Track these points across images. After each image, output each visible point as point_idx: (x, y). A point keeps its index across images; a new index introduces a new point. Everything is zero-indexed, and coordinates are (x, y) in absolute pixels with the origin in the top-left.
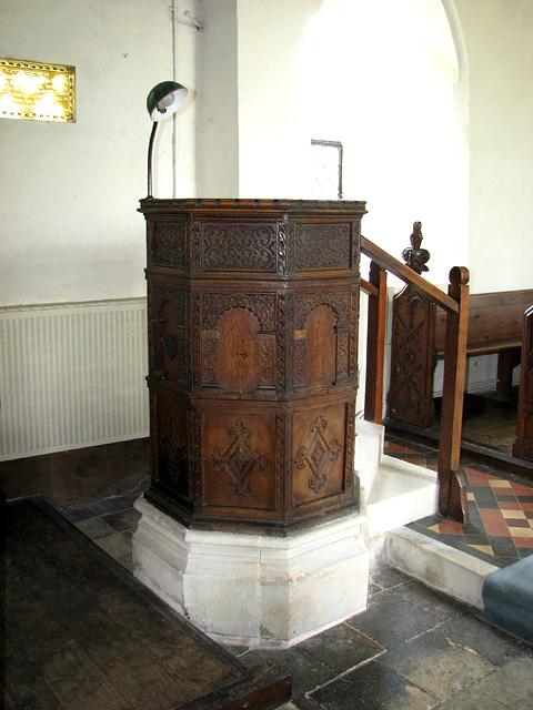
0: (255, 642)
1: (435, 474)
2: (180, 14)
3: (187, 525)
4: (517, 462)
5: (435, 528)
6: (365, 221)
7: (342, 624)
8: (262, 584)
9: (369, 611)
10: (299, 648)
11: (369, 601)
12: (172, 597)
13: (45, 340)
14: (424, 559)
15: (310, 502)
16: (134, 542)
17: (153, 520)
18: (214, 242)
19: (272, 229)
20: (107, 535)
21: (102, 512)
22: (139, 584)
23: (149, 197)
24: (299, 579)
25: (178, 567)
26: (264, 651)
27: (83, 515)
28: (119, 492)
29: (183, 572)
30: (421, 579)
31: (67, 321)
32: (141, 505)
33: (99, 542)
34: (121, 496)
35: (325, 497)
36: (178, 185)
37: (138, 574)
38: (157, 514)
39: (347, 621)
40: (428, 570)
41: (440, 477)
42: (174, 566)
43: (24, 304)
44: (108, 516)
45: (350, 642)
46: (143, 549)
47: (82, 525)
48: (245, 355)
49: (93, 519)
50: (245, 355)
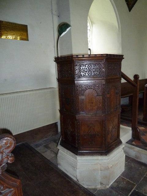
0: (99, 187)
1: (131, 128)
2: (54, 12)
3: (77, 155)
4: (144, 122)
5: (134, 143)
6: (123, 63)
7: (120, 176)
8: (101, 170)
9: (125, 170)
10: (112, 187)
11: (125, 169)
12: (72, 175)
13: (25, 101)
14: (134, 153)
15: (112, 143)
16: (58, 158)
17: (64, 152)
18: (82, 69)
19: (100, 64)
20: (46, 151)
21: (43, 144)
22: (60, 170)
23: (58, 57)
24: (111, 167)
25: (74, 167)
26: (102, 190)
27: (37, 146)
28: (46, 137)
29: (77, 169)
30: (134, 158)
31: (31, 95)
32: (60, 147)
33: (43, 154)
34: (47, 138)
35: (114, 141)
36: (63, 53)
37: (59, 167)
38: (66, 150)
39: (121, 175)
40: (136, 156)
41: (132, 129)
42: (73, 167)
43: (18, 91)
44: (45, 145)
45: (125, 183)
46: (61, 160)
47: (38, 149)
48: (92, 103)
49: (41, 147)
50: (92, 103)
